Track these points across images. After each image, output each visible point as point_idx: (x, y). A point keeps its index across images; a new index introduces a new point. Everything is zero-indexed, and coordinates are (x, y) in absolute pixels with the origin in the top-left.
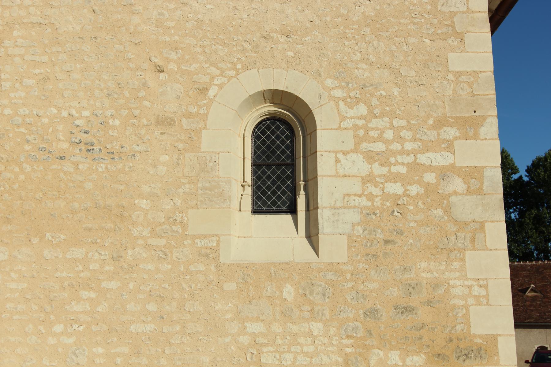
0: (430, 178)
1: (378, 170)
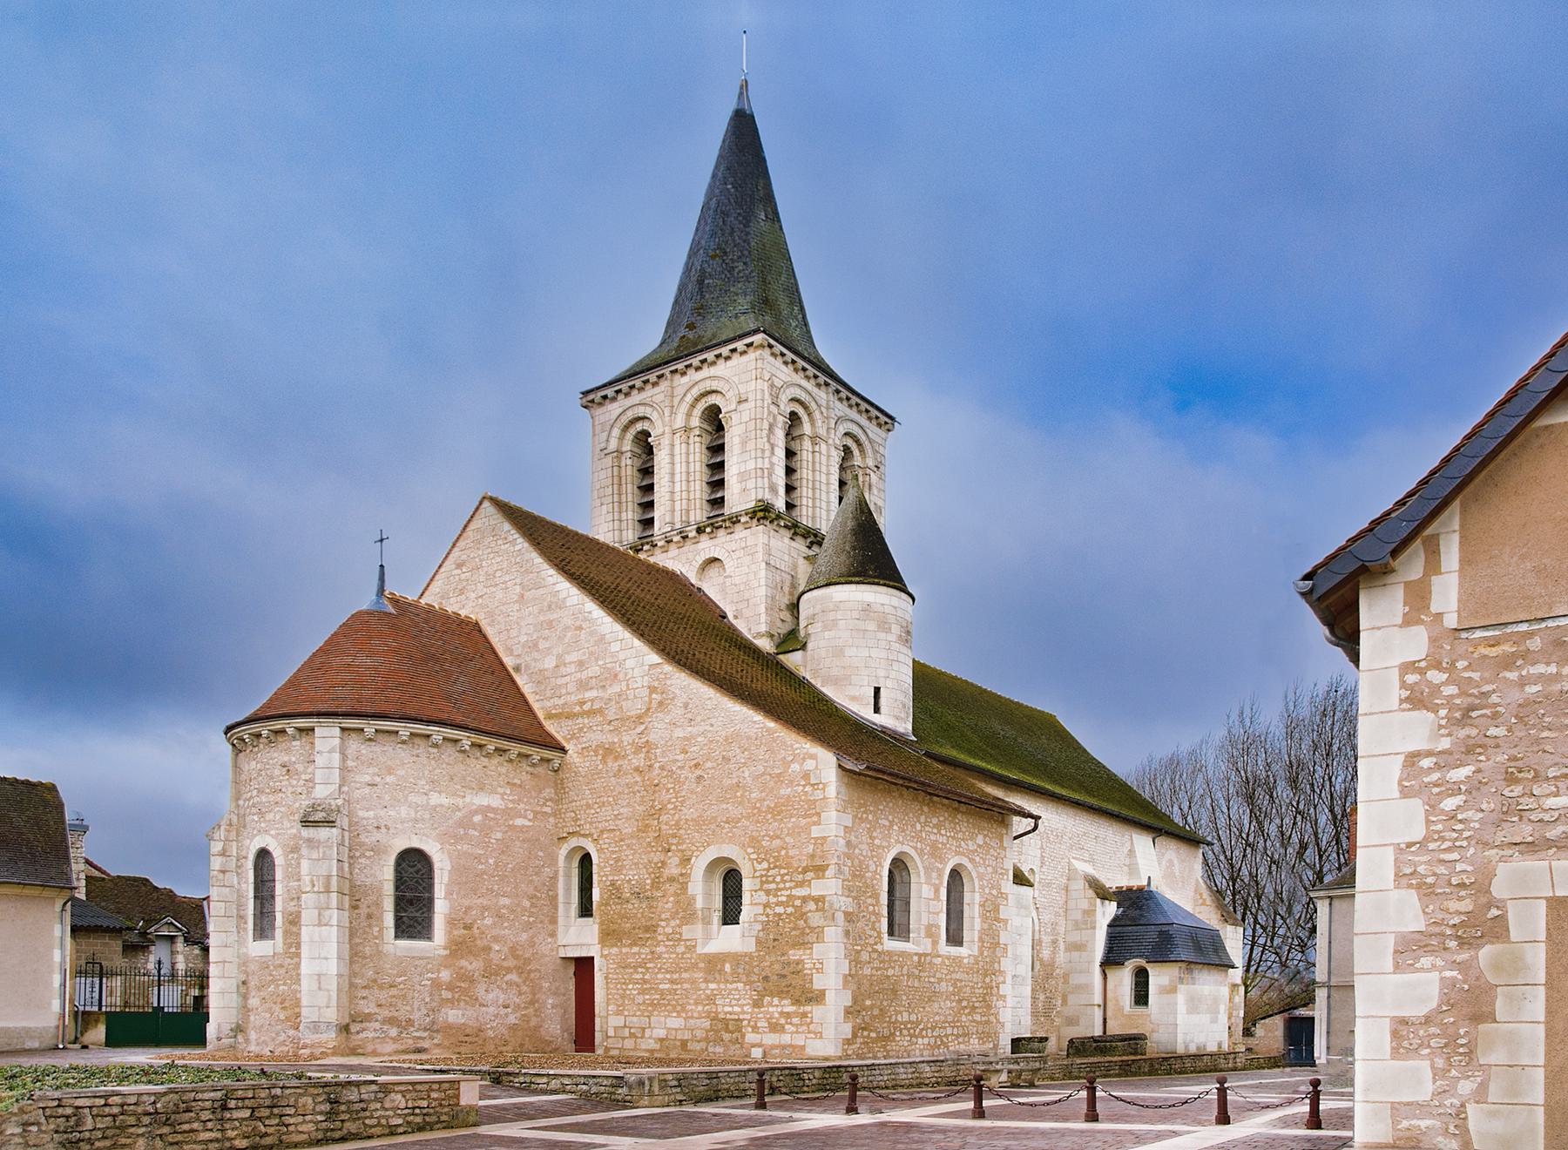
0: (798, 903)
1: (773, 900)
